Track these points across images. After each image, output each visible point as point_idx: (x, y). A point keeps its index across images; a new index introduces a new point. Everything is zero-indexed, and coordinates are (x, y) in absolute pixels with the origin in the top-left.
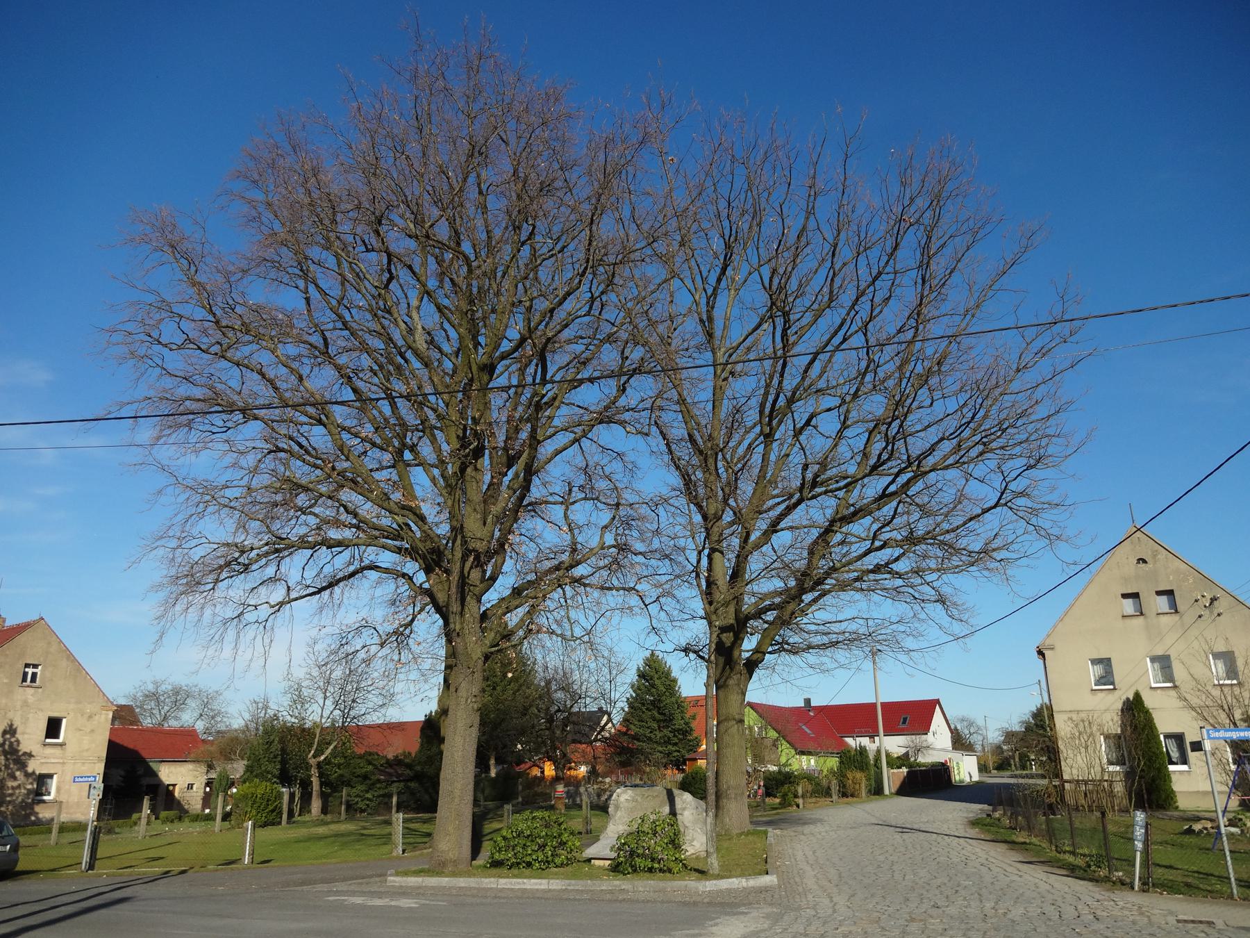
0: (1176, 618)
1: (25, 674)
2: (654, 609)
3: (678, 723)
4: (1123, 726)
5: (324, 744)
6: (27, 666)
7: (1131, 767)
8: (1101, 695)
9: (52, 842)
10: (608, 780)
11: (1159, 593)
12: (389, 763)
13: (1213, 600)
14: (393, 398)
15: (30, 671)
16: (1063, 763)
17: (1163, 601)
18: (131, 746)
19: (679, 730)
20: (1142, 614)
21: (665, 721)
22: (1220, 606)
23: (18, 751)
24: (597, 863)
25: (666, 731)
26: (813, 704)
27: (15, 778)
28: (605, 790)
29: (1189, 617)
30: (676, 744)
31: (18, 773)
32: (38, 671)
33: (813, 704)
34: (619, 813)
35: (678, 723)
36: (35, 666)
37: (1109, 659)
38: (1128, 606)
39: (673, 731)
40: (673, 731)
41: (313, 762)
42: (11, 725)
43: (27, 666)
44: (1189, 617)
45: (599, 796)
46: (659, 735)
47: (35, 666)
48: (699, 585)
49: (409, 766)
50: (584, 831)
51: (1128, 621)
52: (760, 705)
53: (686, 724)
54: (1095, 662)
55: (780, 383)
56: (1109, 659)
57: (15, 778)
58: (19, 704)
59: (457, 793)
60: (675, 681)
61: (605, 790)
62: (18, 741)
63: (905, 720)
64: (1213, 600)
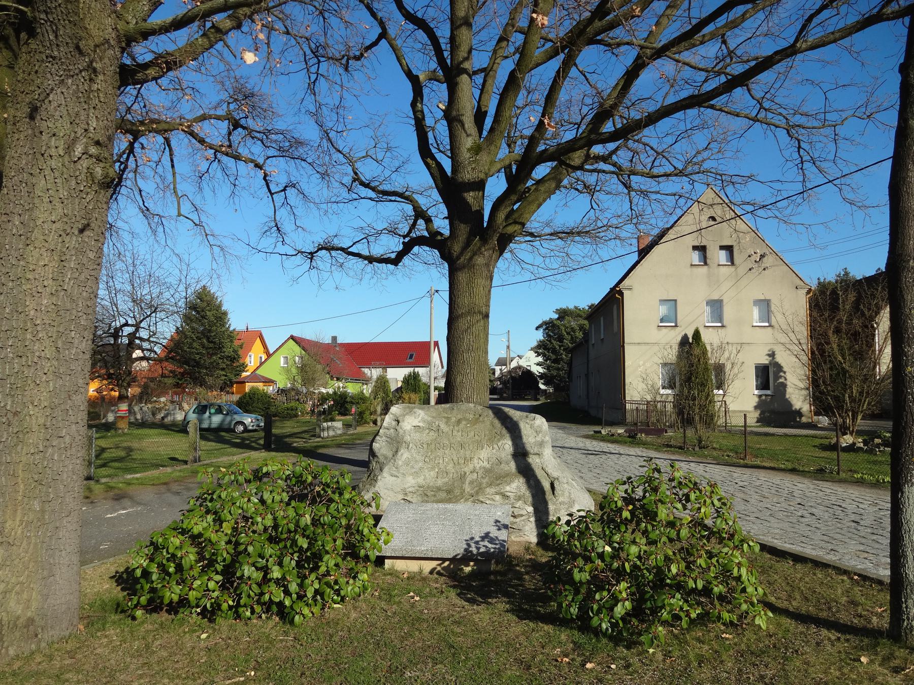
0: (732, 269)
2: (279, 198)
3: (228, 351)
4: (680, 356)
7: (681, 392)
8: (664, 330)
10: (163, 399)
11: (722, 248)
13: (762, 256)
17: (723, 254)
20: (706, 264)
22: (769, 260)
24: (400, 565)
26: (339, 342)
28: (160, 410)
29: (742, 269)
30: (223, 369)
33: (339, 342)
34: (404, 455)
35: (228, 351)
37: (675, 301)
38: (696, 257)
44: (742, 269)
45: (154, 414)
50: (190, 458)
51: (695, 269)
52: (304, 340)
53: (235, 351)
54: (663, 301)
55: (259, 132)
56: (675, 301)
59: (36, 417)
60: (225, 313)
61: (160, 410)
63: (411, 357)
64: (762, 256)
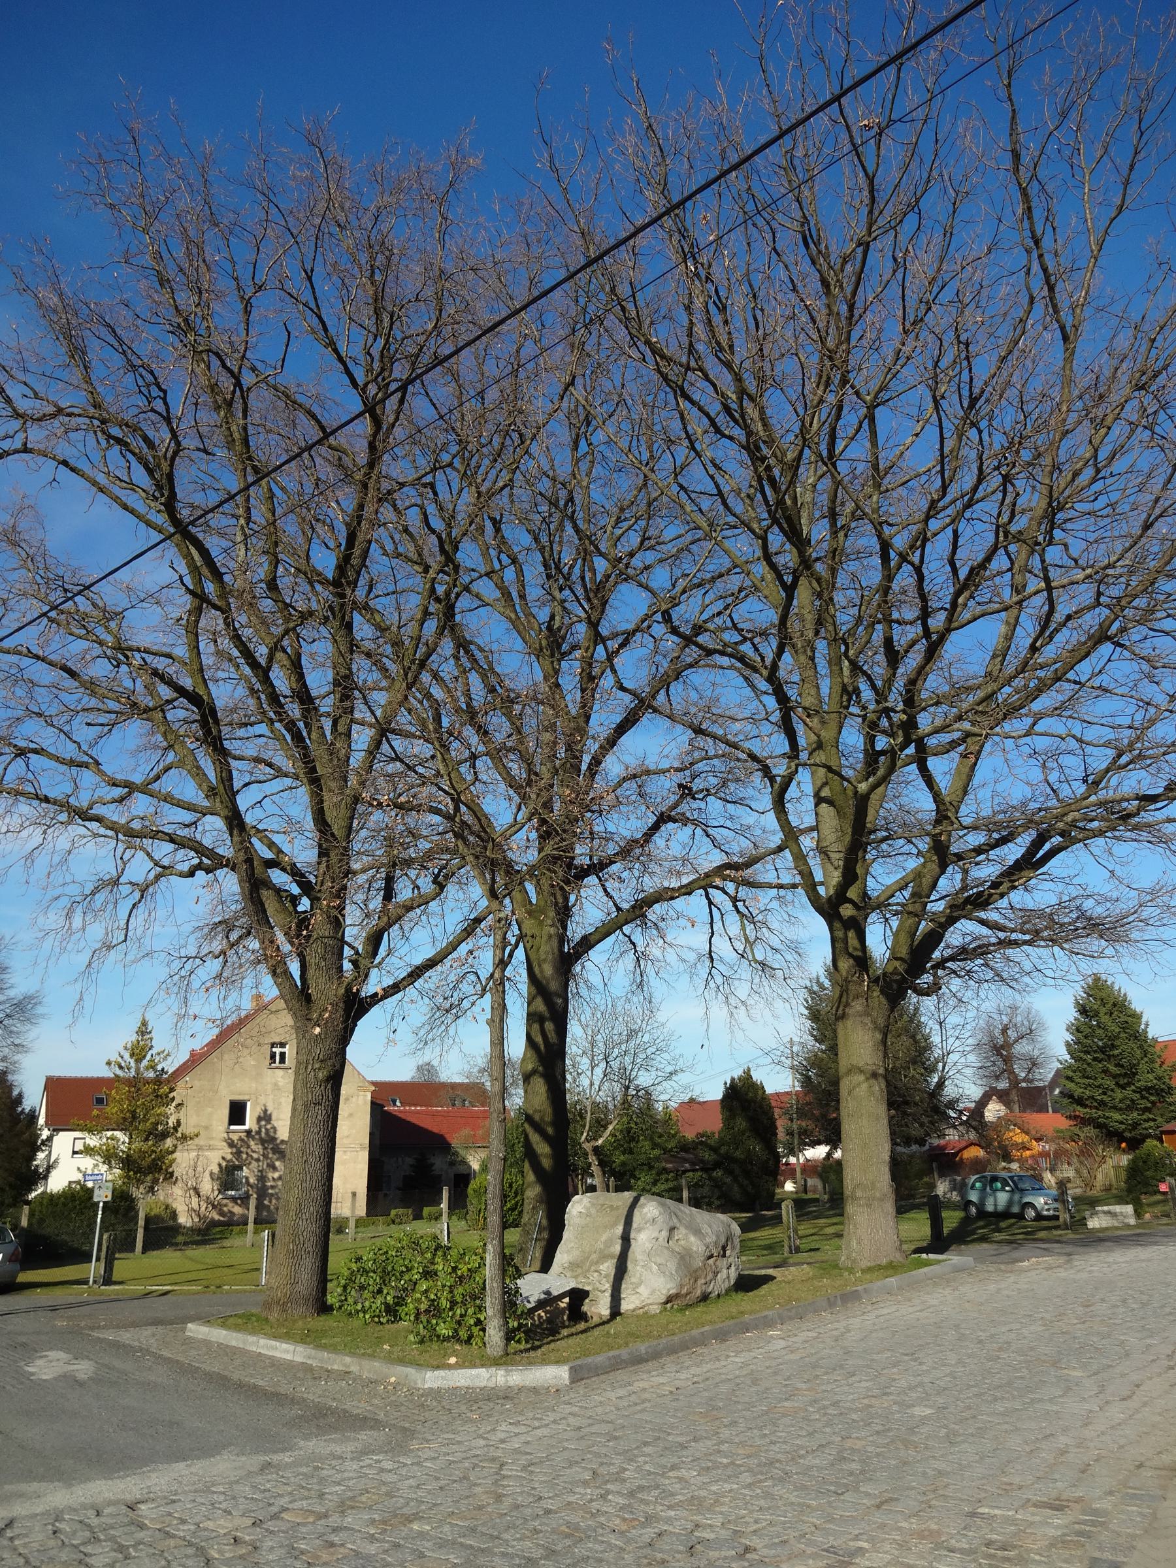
1: (273, 1056)
5: (600, 1125)
6: (273, 1045)
9: (249, 1244)
12: (685, 1147)
14: (336, 583)
15: (277, 1050)
16: (248, 1348)
18: (435, 1130)
19: (1147, 1089)
21: (1125, 1075)
23: (274, 1139)
25: (1128, 1092)
27: (274, 1168)
31: (277, 1164)
32: (286, 1050)
35: (1145, 1078)
36: (283, 1045)
39: (1139, 1091)
40: (1139, 1091)
41: (588, 1147)
42: (265, 1111)
43: (273, 1045)
46: (1119, 1094)
47: (283, 1045)
48: (481, 650)
49: (714, 1149)
53: (1159, 1078)
57: (274, 1168)
58: (269, 1087)
60: (1137, 1017)
62: (274, 1129)
